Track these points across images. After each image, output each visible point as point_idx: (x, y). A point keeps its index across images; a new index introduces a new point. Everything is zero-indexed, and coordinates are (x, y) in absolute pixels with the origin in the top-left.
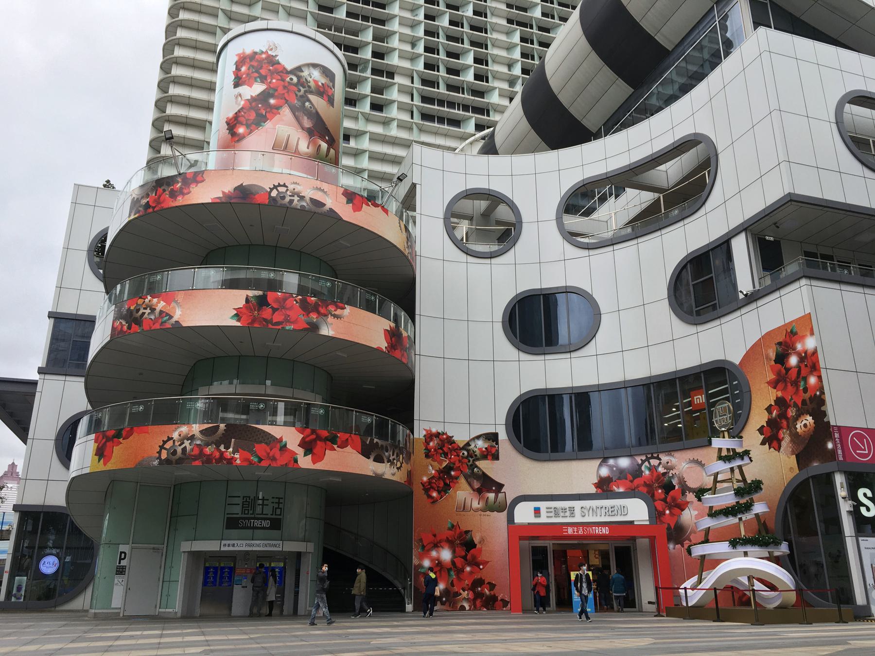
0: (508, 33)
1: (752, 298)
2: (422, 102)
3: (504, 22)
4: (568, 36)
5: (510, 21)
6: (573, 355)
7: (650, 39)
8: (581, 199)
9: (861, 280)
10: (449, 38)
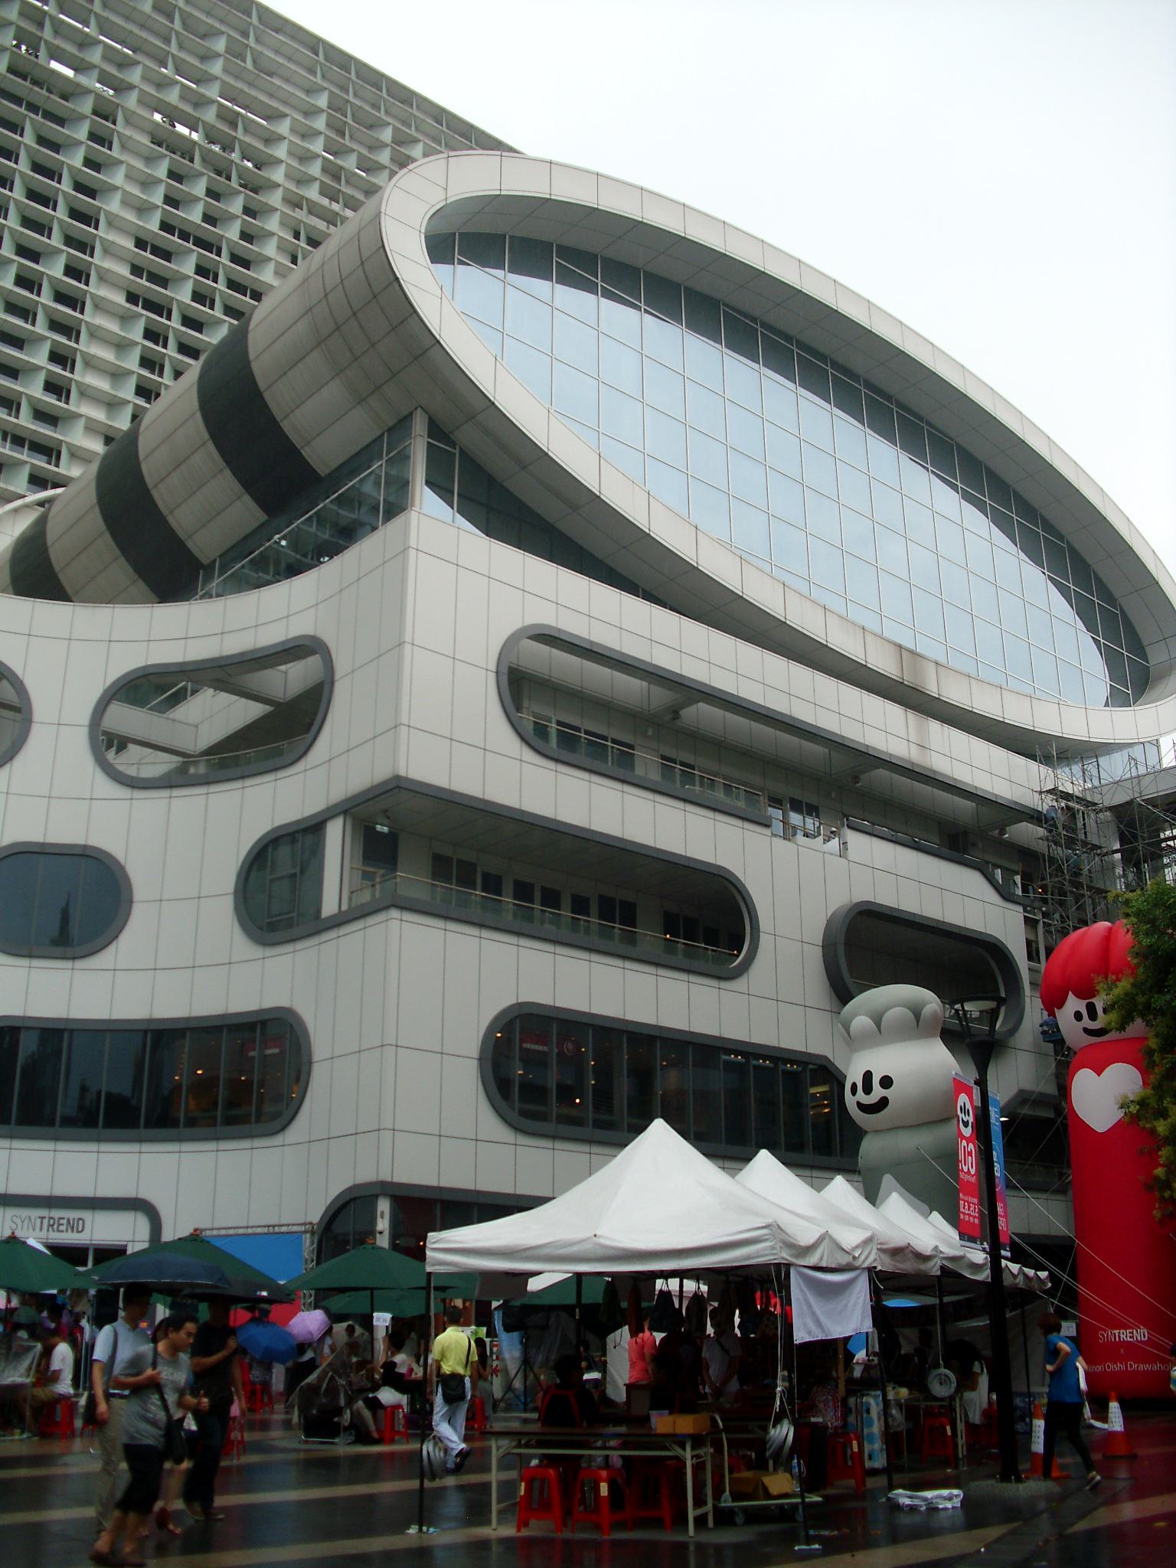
0: (125, 319)
1: (339, 921)
2: (75, 190)
3: (120, 299)
4: (180, 392)
5: (132, 298)
6: (79, 964)
7: (181, 544)
8: (154, 687)
9: (945, 851)
10: (235, 258)
